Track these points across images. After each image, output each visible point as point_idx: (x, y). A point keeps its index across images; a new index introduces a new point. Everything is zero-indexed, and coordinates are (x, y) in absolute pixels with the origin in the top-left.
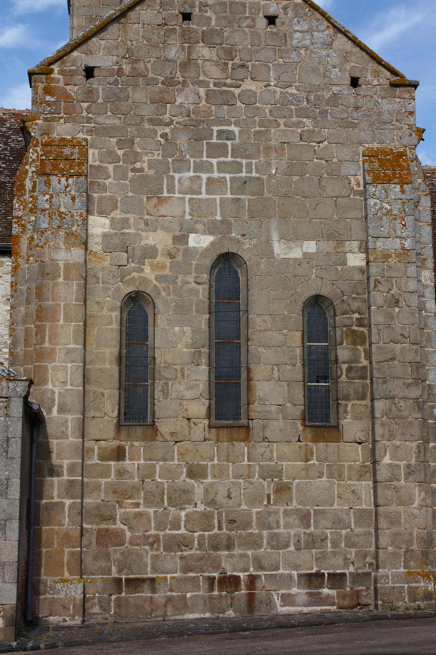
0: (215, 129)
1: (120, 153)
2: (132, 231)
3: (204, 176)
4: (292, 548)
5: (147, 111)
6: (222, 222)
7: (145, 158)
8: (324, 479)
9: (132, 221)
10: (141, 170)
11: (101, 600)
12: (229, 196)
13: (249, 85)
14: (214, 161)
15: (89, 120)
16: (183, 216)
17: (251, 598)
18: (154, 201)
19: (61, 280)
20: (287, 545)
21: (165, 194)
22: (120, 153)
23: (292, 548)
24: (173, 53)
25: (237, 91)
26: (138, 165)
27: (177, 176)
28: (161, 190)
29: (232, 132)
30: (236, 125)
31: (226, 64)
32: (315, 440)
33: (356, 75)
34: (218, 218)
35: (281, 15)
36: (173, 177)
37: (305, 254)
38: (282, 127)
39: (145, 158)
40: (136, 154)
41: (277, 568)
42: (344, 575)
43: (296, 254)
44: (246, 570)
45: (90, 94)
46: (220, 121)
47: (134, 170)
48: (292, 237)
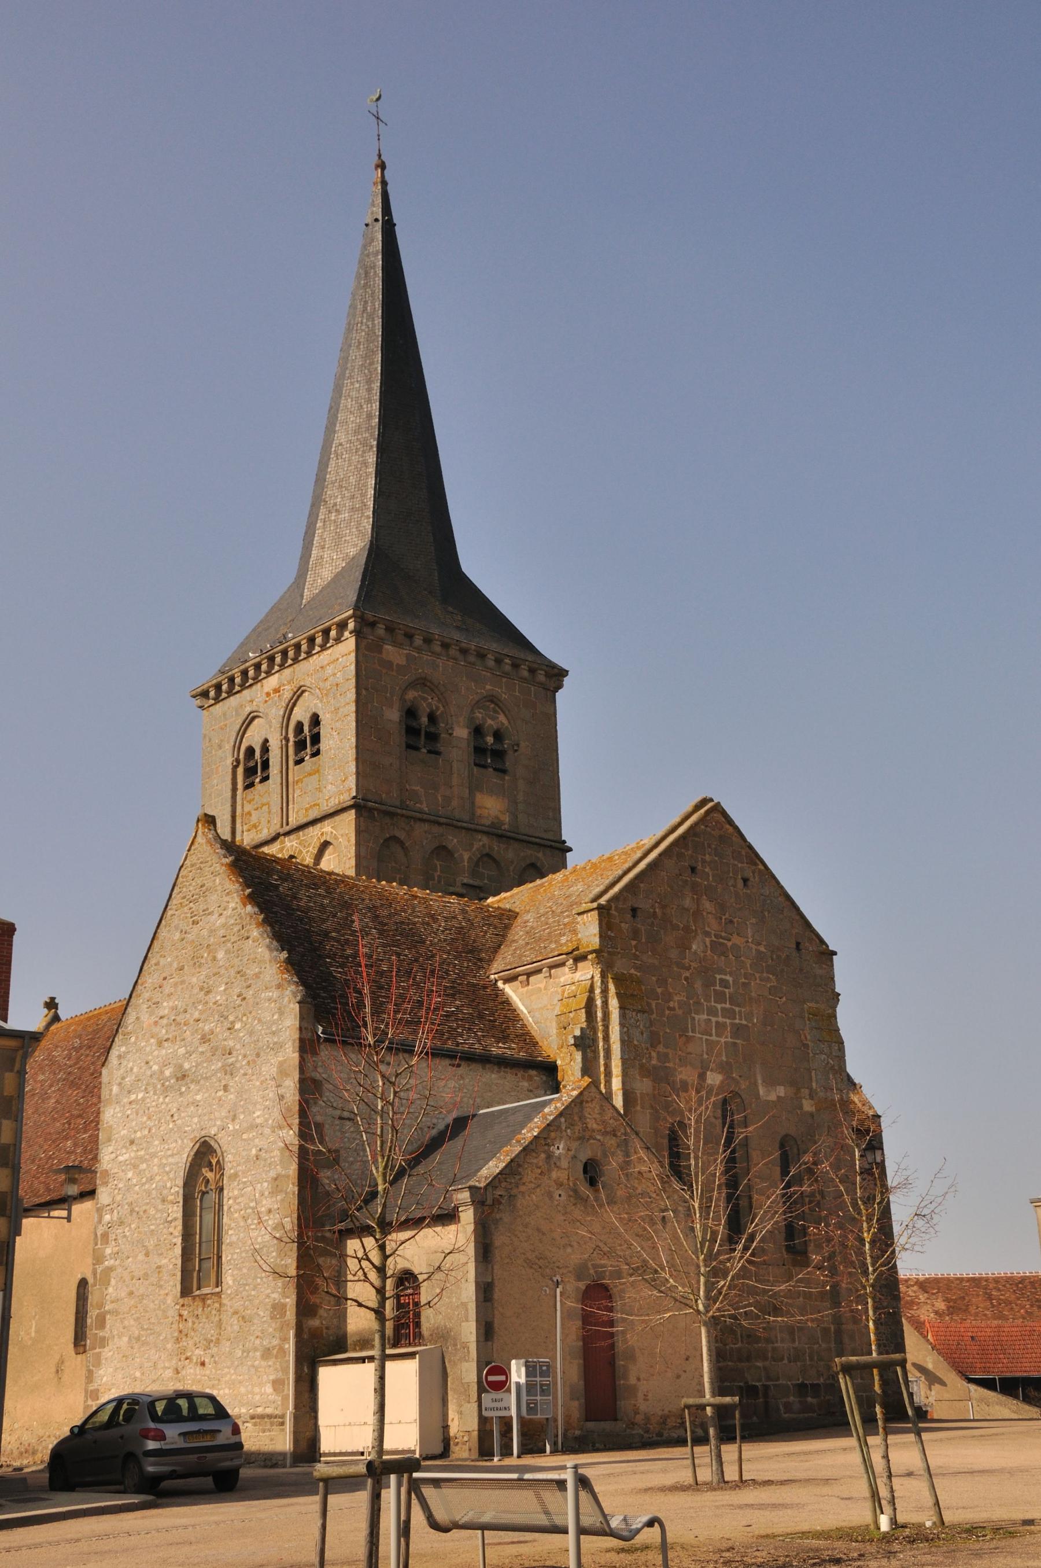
0: (718, 977)
1: (659, 990)
2: (671, 1065)
3: (714, 1019)
4: (786, 1361)
5: (674, 954)
6: (727, 1062)
7: (676, 998)
8: (801, 1299)
9: (670, 1056)
10: (673, 1009)
11: (551, 1423)
12: (729, 1040)
13: (736, 940)
14: (719, 1006)
15: (636, 957)
16: (702, 1055)
17: (766, 1403)
18: (684, 1039)
19: (638, 1108)
20: (782, 1359)
21: (690, 1034)
22: (659, 990)
23: (786, 1361)
24: (687, 902)
25: (729, 944)
26: (671, 1004)
27: (697, 1017)
28: (686, 1030)
29: (728, 981)
30: (731, 974)
31: (721, 919)
32: (794, 1266)
33: (800, 940)
34: (724, 1059)
35: (752, 879)
36: (694, 1018)
37: (778, 1097)
38: (758, 981)
39: (676, 998)
40: (670, 994)
41: (778, 1379)
42: (818, 1385)
43: (773, 1097)
44: (759, 1380)
45: (636, 934)
46: (721, 971)
47: (669, 1008)
48: (771, 1082)
